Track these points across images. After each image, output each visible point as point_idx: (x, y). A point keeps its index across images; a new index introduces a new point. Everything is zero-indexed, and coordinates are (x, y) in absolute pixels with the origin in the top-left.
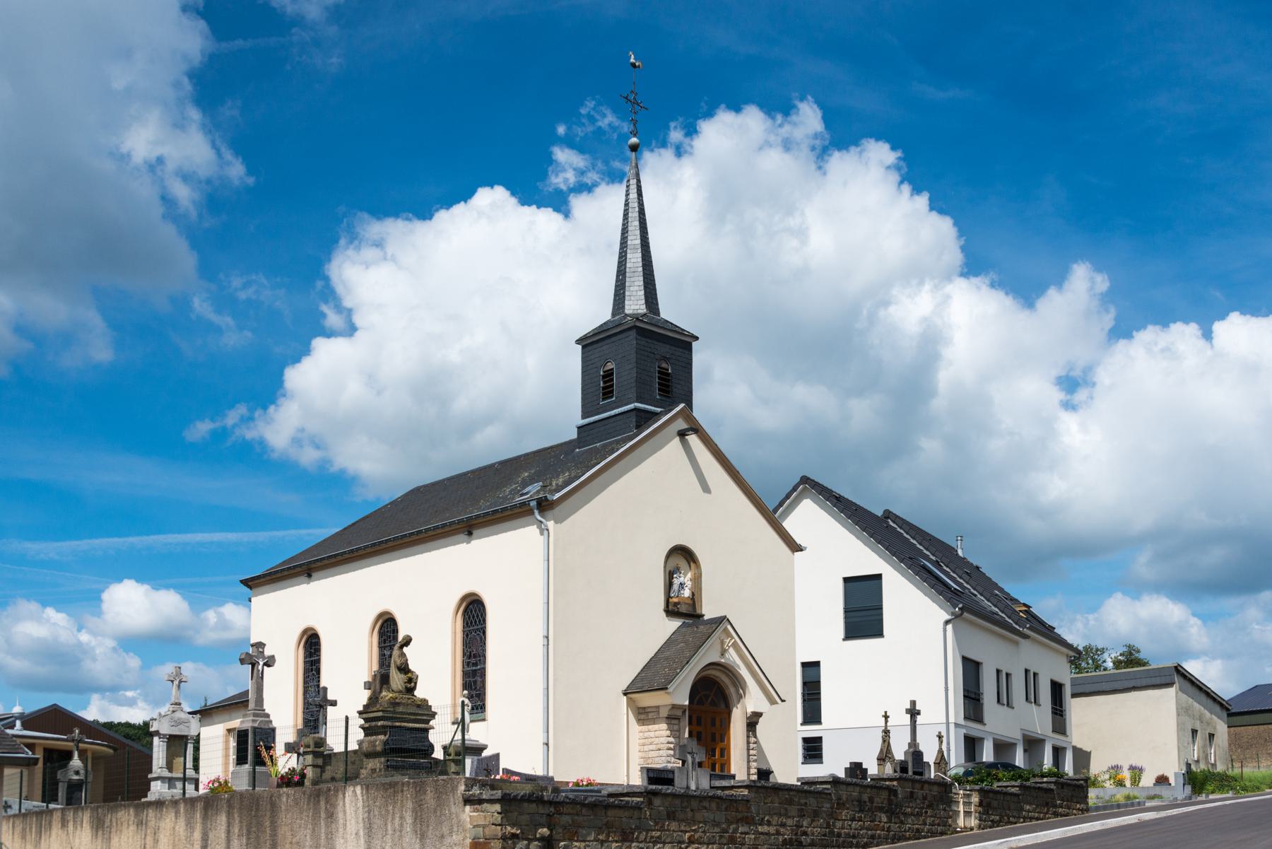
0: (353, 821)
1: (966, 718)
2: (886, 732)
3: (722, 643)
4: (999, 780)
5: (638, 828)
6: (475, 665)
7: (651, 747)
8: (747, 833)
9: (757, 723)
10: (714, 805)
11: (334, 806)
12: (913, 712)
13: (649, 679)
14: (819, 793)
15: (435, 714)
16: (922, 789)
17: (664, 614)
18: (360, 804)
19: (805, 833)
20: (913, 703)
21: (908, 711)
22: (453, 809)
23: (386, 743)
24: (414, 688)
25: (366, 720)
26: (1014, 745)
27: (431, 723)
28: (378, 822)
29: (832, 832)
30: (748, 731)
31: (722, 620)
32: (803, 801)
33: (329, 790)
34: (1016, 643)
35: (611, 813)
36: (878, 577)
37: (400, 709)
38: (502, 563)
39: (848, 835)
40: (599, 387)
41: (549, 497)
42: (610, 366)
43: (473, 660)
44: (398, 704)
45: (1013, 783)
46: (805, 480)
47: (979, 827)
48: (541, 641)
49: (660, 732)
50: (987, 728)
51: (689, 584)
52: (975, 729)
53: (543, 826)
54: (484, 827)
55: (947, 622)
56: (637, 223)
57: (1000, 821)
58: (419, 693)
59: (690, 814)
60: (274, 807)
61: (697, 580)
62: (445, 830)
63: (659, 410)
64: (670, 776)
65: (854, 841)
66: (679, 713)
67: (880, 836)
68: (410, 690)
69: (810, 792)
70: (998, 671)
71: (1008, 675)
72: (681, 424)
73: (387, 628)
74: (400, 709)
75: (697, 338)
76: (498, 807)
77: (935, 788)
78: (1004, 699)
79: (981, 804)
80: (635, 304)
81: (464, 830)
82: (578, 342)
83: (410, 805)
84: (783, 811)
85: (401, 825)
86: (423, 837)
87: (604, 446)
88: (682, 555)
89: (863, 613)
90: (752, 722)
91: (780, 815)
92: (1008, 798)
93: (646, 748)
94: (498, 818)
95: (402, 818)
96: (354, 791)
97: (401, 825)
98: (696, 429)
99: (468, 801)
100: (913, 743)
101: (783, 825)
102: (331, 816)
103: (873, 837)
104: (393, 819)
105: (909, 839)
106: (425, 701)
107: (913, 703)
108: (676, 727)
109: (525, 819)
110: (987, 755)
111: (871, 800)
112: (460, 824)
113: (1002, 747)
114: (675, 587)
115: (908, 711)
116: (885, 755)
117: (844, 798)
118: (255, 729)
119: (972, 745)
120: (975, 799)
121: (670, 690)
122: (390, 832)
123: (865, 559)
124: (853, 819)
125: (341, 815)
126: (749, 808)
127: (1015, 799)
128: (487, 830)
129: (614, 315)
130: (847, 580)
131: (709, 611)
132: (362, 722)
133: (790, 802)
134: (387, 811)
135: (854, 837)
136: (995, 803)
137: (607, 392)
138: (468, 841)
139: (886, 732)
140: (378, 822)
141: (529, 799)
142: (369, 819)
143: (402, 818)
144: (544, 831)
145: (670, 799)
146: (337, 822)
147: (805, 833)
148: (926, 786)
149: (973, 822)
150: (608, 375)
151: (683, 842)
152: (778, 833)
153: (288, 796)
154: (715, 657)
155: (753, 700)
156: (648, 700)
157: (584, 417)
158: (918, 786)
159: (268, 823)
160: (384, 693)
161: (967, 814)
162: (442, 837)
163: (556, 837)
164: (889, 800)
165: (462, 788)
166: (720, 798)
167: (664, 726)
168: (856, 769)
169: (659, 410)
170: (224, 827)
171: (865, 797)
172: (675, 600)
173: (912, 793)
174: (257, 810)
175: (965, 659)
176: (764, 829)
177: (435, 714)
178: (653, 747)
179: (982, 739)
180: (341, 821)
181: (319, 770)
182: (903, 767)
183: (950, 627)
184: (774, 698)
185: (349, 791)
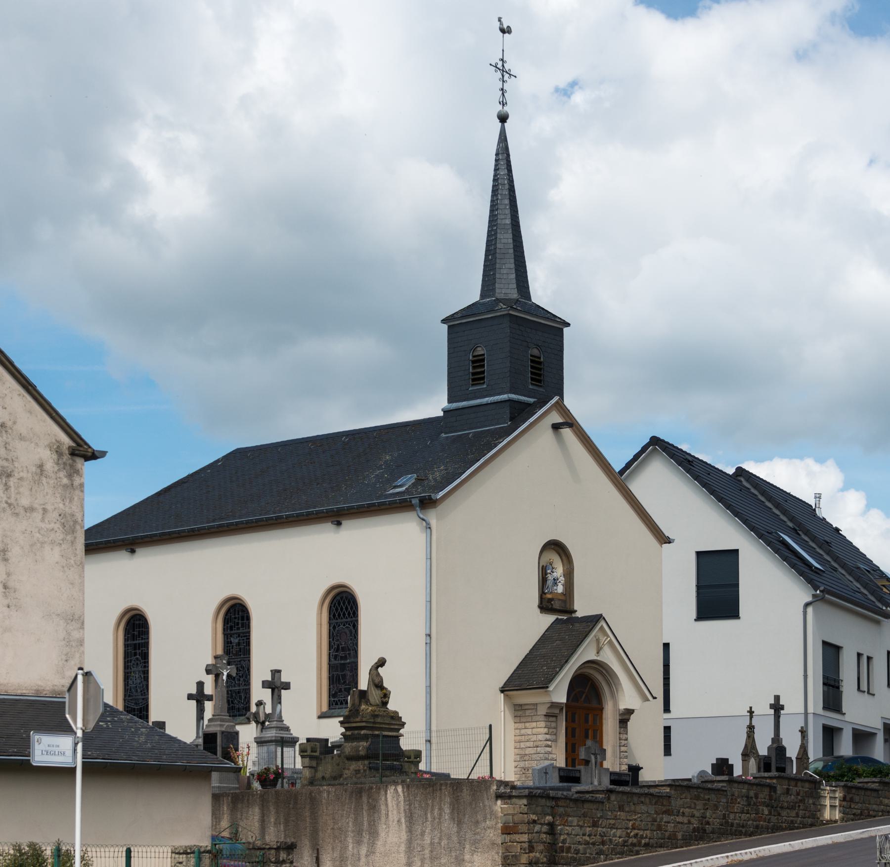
0: (395, 812)
1: (825, 708)
2: (751, 728)
3: (598, 641)
4: (860, 776)
5: (601, 817)
6: (345, 658)
7: (528, 744)
8: (669, 822)
9: (628, 720)
10: (647, 800)
11: (377, 800)
12: (777, 707)
13: (526, 678)
14: (718, 790)
15: (405, 723)
16: (796, 786)
17: (538, 610)
18: (402, 798)
19: (708, 823)
20: (777, 698)
21: (772, 706)
22: (486, 803)
23: (368, 749)
24: (387, 703)
25: (347, 729)
26: (873, 735)
27: (401, 731)
28: (418, 812)
29: (727, 822)
30: (620, 727)
31: (596, 619)
32: (707, 797)
33: (372, 788)
34: (878, 622)
35: (586, 805)
36: (734, 554)
37: (379, 720)
38: (379, 556)
39: (738, 825)
40: (467, 369)
41: (433, 496)
42: (480, 351)
43: (341, 654)
44: (377, 716)
45: (874, 779)
46: (655, 441)
47: (842, 819)
48: (423, 639)
49: (538, 729)
50: (847, 718)
51: (562, 579)
52: (832, 719)
53: (549, 815)
54: (513, 815)
55: (807, 605)
56: (507, 202)
57: (861, 814)
58: (391, 706)
59: (633, 808)
60: (314, 802)
61: (569, 575)
62: (480, 817)
63: (532, 400)
64: (577, 775)
65: (744, 830)
66: (557, 711)
67: (762, 827)
68: (385, 704)
69: (709, 789)
70: (859, 655)
71: (869, 659)
72: (556, 418)
73: (235, 619)
74: (379, 720)
75: (568, 325)
76: (525, 801)
77: (807, 785)
78: (864, 688)
79: (844, 799)
80: (507, 289)
81: (496, 818)
82: (444, 321)
83: (448, 799)
84: (693, 806)
85: (440, 815)
86: (460, 823)
87: (477, 436)
88: (556, 547)
89: (717, 592)
90: (625, 717)
91: (690, 807)
92: (868, 793)
93: (522, 745)
94: (525, 809)
95: (440, 809)
96: (396, 790)
97: (440, 815)
98: (570, 423)
99: (499, 796)
100: (777, 739)
101: (693, 816)
102: (374, 808)
103: (757, 827)
104: (432, 810)
105: (785, 829)
106: (397, 713)
107: (777, 698)
108: (553, 725)
109: (539, 809)
110: (845, 748)
111: (756, 796)
112: (492, 813)
113: (861, 737)
114: (550, 582)
115: (772, 706)
116: (749, 751)
117: (736, 794)
118: (223, 732)
119: (830, 734)
120: (839, 794)
121: (551, 689)
122: (430, 819)
123: (722, 531)
124: (742, 812)
125: (383, 807)
126: (670, 802)
127: (875, 794)
128: (516, 818)
129: (483, 295)
130: (699, 554)
131: (582, 608)
132: (343, 730)
133: (697, 798)
134: (427, 804)
135: (743, 826)
136: (857, 798)
137: (478, 378)
138: (500, 825)
139: (751, 728)
140: (418, 812)
141: (541, 796)
142: (410, 810)
143: (440, 809)
144: (549, 818)
145: (620, 795)
146: (379, 811)
147: (708, 823)
148: (799, 784)
149: (837, 815)
150: (478, 362)
151: (627, 828)
152: (689, 822)
153: (329, 792)
154: (591, 655)
155: (628, 698)
156: (526, 697)
157: (449, 401)
158: (793, 783)
159: (307, 814)
160: (363, 707)
161: (833, 807)
162: (477, 822)
163: (557, 823)
164: (770, 796)
165: (495, 787)
166: (652, 795)
167: (543, 724)
168: (722, 766)
169: (532, 400)
170: (257, 818)
171: (752, 793)
172: (549, 596)
173: (788, 790)
174: (296, 803)
175: (825, 644)
176: (680, 819)
177: (405, 723)
178: (531, 744)
179: (840, 730)
180: (383, 812)
181: (313, 770)
182: (765, 764)
183: (810, 610)
184: (645, 696)
185: (391, 790)
